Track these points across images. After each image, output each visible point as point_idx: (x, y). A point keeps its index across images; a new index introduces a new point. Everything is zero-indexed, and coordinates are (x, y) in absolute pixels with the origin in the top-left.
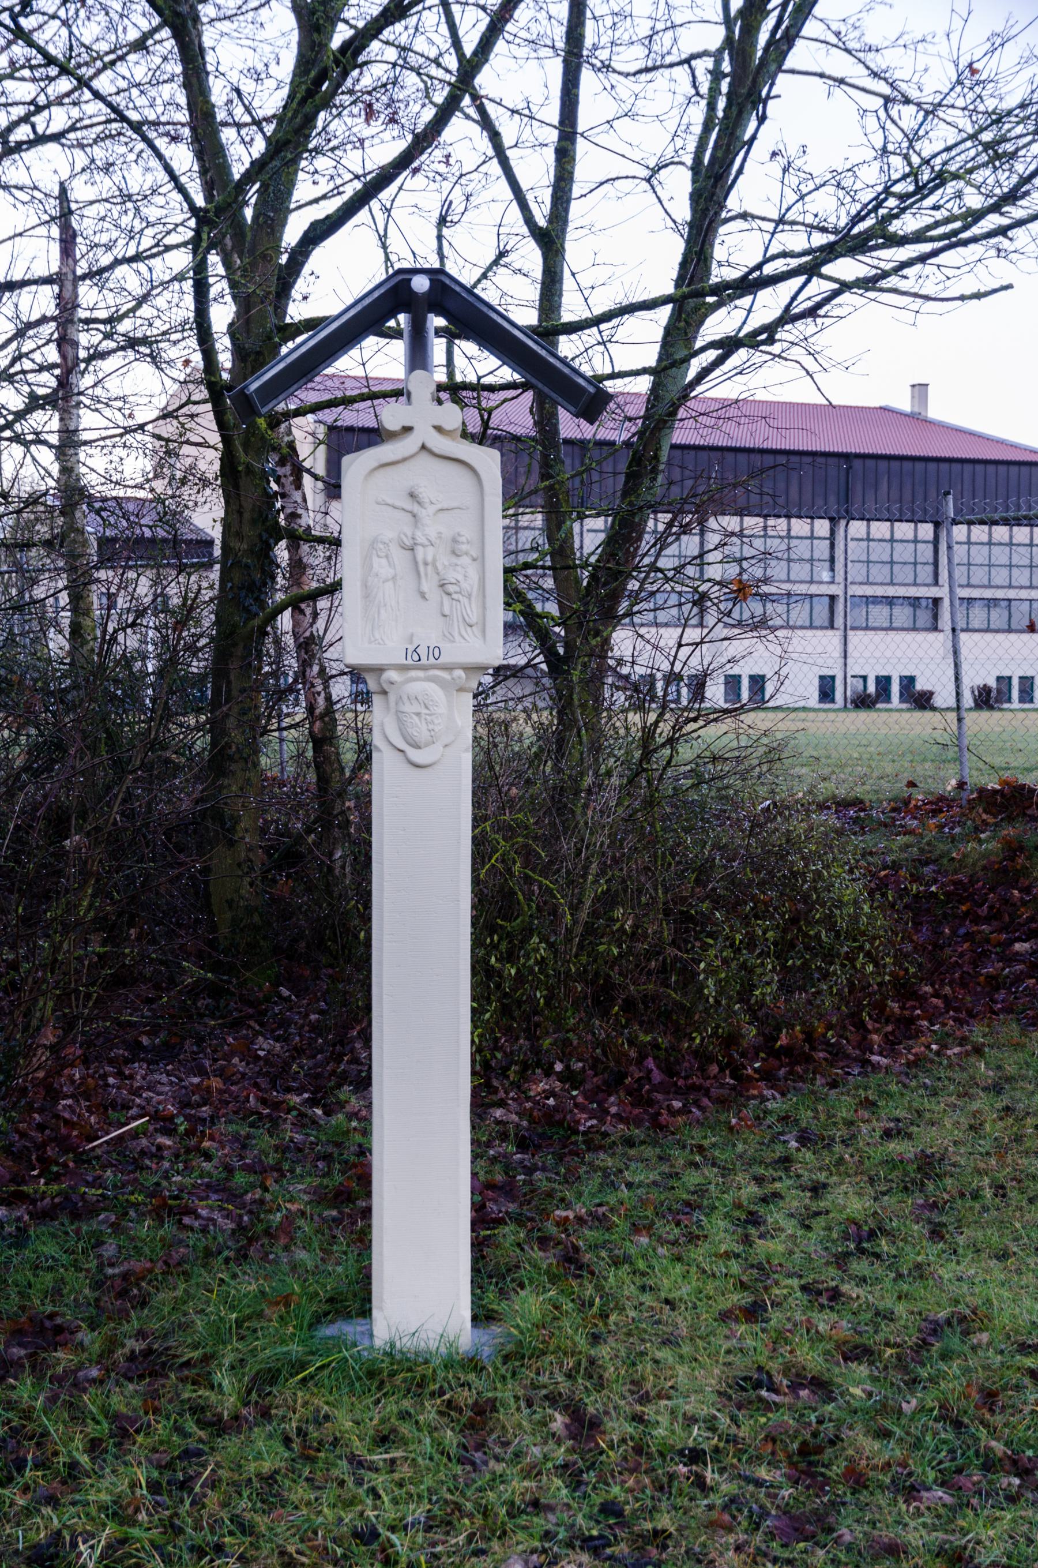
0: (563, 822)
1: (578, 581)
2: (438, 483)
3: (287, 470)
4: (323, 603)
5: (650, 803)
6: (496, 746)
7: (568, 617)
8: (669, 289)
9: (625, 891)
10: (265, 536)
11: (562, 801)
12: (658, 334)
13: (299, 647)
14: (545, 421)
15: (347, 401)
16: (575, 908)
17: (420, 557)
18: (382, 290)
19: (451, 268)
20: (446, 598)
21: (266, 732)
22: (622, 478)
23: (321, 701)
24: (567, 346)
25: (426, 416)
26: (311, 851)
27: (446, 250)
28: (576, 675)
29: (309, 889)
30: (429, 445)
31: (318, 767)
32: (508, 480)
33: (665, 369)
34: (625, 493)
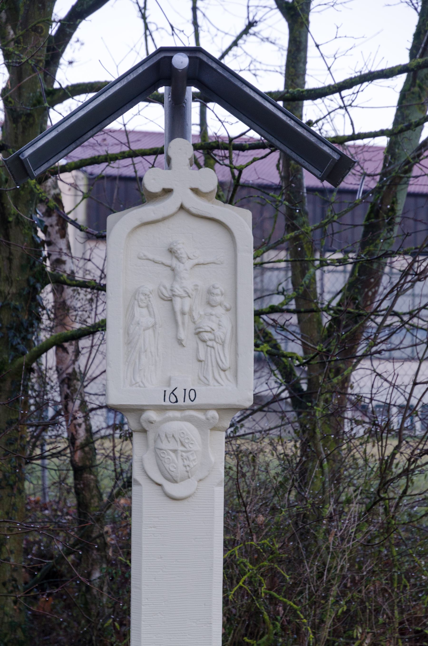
0: (306, 547)
1: (320, 322)
2: (195, 241)
3: (53, 220)
4: (84, 343)
5: (387, 529)
6: (244, 475)
7: (311, 359)
8: (404, 59)
9: (364, 611)
10: (32, 281)
11: (304, 527)
12: (395, 98)
13: (62, 382)
14: (290, 175)
15: (109, 159)
16: (317, 628)
17: (178, 307)
18: (145, 67)
19: (204, 45)
20: (201, 345)
21: (30, 459)
22: (361, 229)
23: (82, 433)
24: (310, 110)
25: (181, 177)
26: (70, 570)
27: (200, 20)
28: (319, 411)
29: (68, 607)
30: (187, 205)
31: (78, 493)
32: (257, 226)
33: (401, 131)
34: (364, 244)
